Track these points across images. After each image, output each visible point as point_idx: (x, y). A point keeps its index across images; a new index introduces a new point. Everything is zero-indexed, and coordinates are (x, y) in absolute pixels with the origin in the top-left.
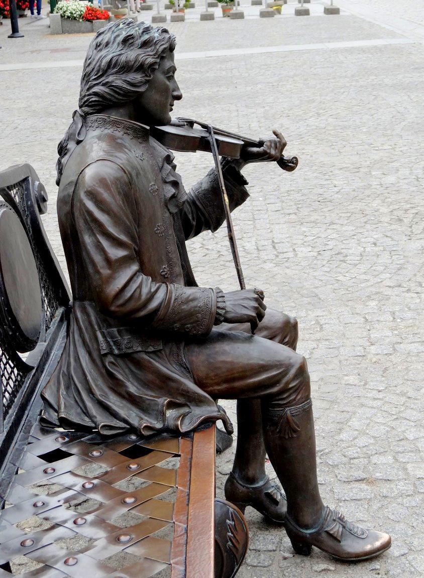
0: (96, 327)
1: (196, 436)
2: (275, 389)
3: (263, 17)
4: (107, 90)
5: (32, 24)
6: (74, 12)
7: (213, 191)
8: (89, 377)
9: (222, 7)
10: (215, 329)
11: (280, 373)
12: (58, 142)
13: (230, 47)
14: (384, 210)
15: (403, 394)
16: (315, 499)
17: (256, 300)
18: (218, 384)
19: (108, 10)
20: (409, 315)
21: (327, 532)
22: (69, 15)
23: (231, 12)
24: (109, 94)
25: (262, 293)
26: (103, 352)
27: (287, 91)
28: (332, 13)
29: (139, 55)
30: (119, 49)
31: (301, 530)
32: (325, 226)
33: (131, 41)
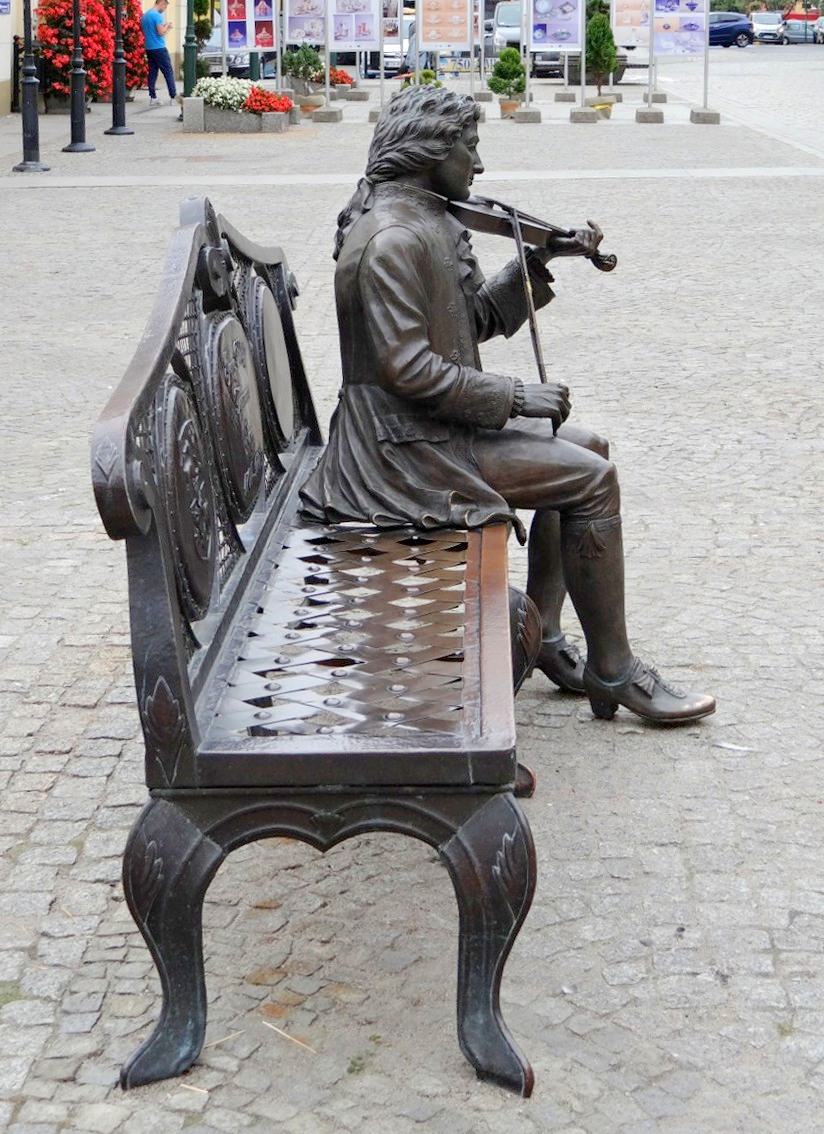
0: (373, 412)
1: (485, 532)
2: (579, 497)
3: (575, 122)
4: (403, 157)
5: (147, 113)
6: (229, 96)
7: (514, 282)
8: (361, 468)
9: (501, 101)
10: (511, 425)
11: (586, 477)
12: (339, 212)
13: (515, 167)
14: (759, 401)
15: (753, 595)
16: (621, 642)
17: (561, 394)
18: (512, 487)
19: (287, 96)
20: (778, 519)
21: (636, 685)
22: (220, 100)
23: (518, 110)
24: (404, 161)
25: (567, 389)
26: (380, 439)
27: (614, 237)
28: (705, 121)
29: (440, 122)
30: (418, 114)
31: (605, 683)
32: (662, 418)
33: (431, 107)
